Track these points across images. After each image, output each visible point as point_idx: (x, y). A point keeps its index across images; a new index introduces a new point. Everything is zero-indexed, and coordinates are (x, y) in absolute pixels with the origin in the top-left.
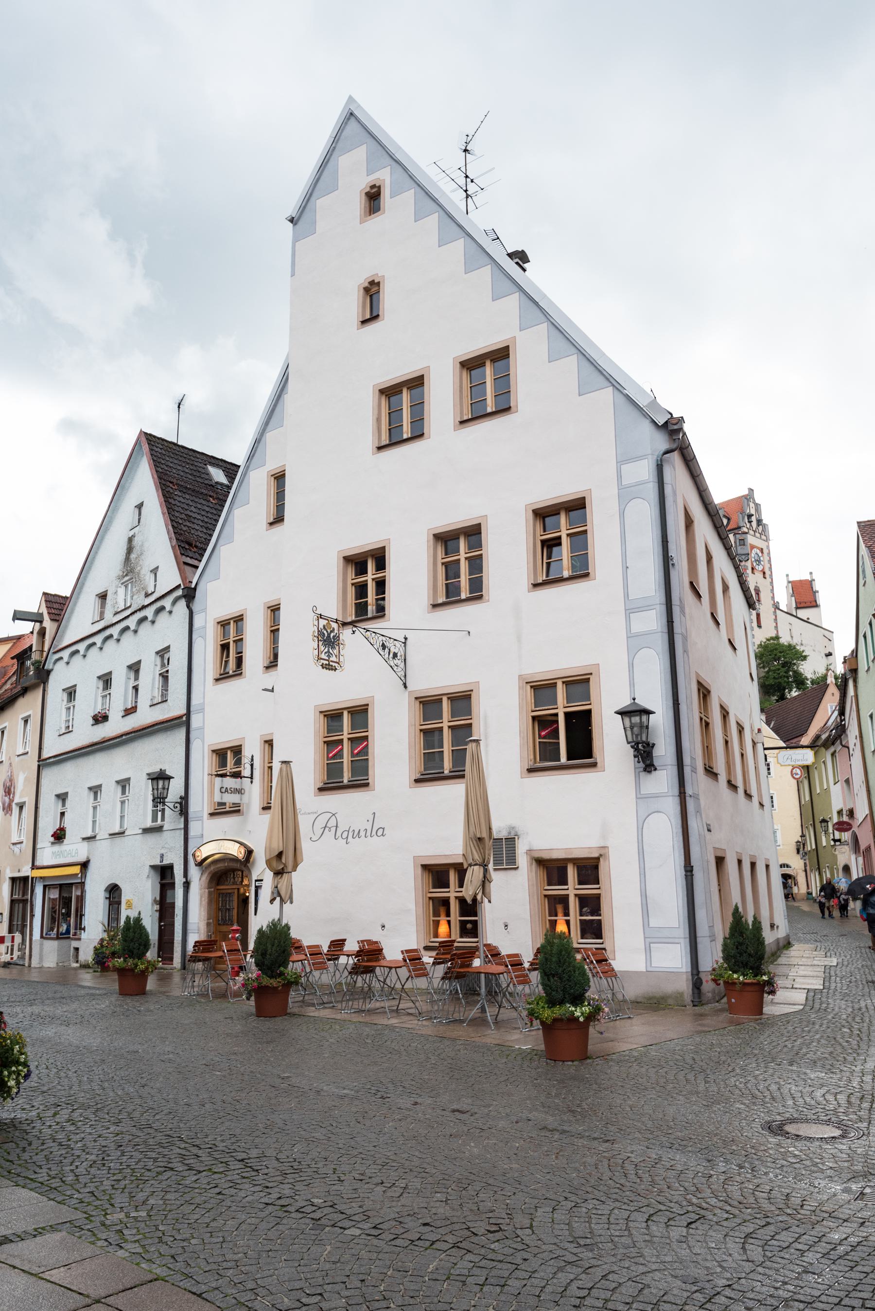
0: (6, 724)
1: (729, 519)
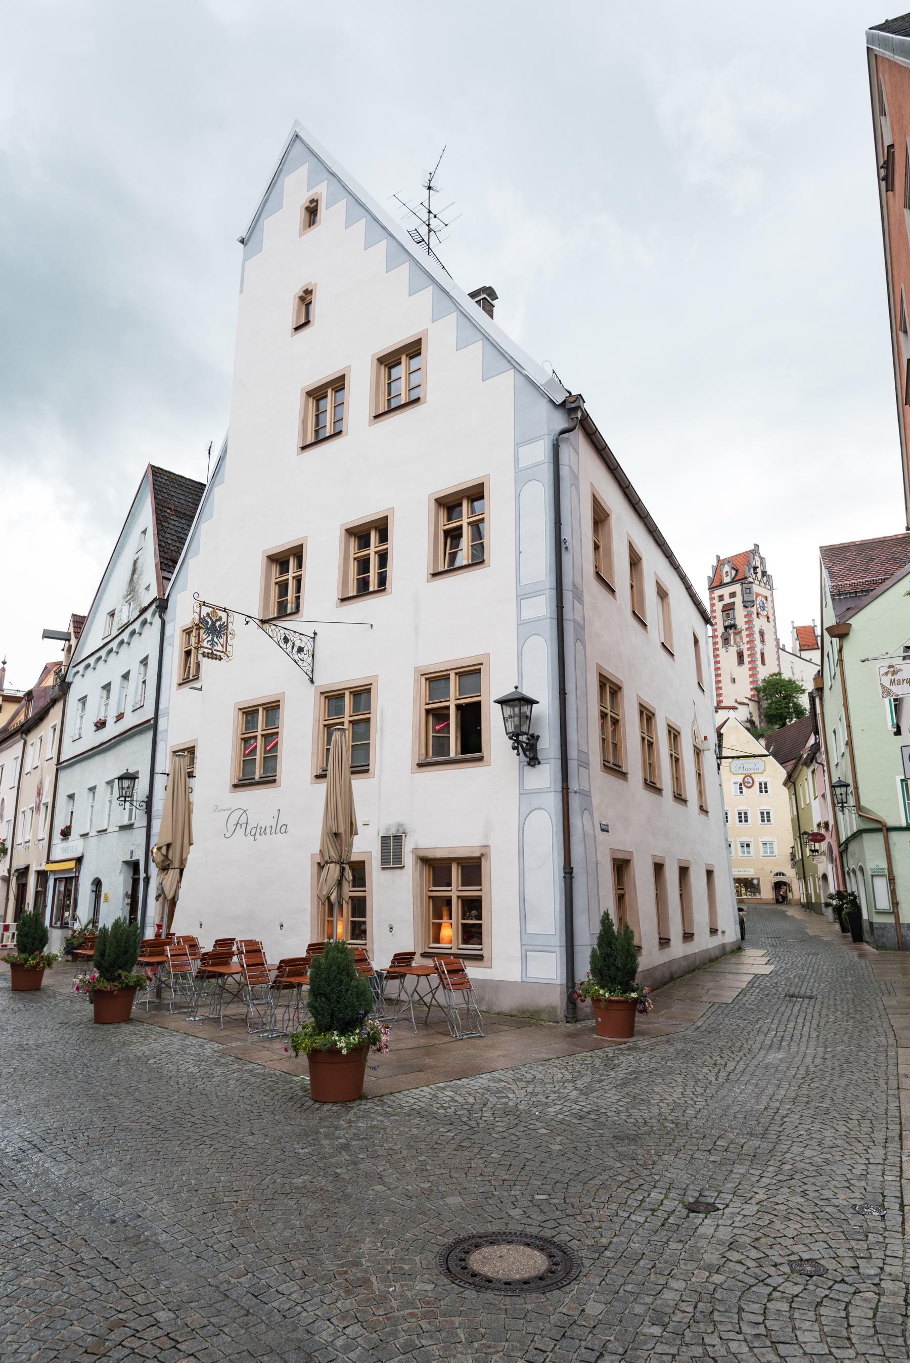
0: (42, 733)
1: (737, 571)
